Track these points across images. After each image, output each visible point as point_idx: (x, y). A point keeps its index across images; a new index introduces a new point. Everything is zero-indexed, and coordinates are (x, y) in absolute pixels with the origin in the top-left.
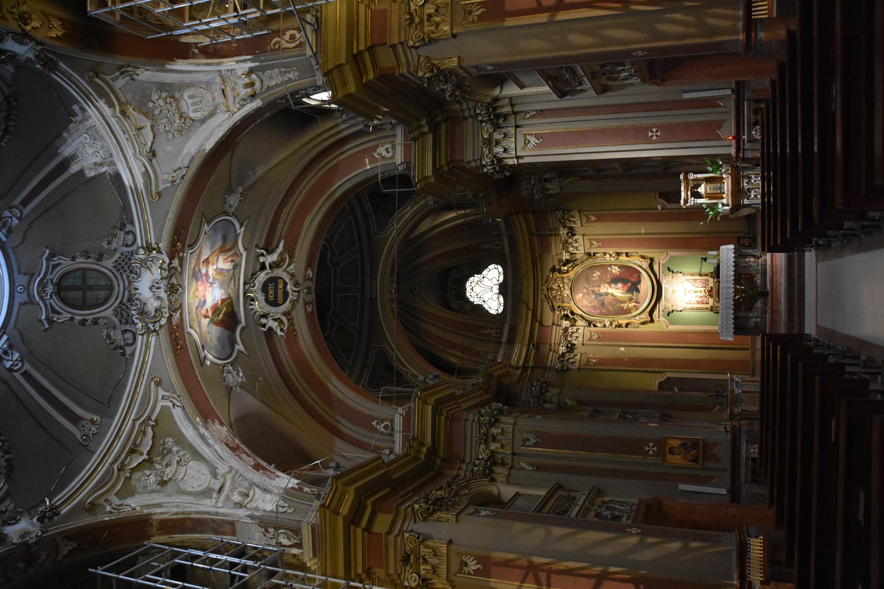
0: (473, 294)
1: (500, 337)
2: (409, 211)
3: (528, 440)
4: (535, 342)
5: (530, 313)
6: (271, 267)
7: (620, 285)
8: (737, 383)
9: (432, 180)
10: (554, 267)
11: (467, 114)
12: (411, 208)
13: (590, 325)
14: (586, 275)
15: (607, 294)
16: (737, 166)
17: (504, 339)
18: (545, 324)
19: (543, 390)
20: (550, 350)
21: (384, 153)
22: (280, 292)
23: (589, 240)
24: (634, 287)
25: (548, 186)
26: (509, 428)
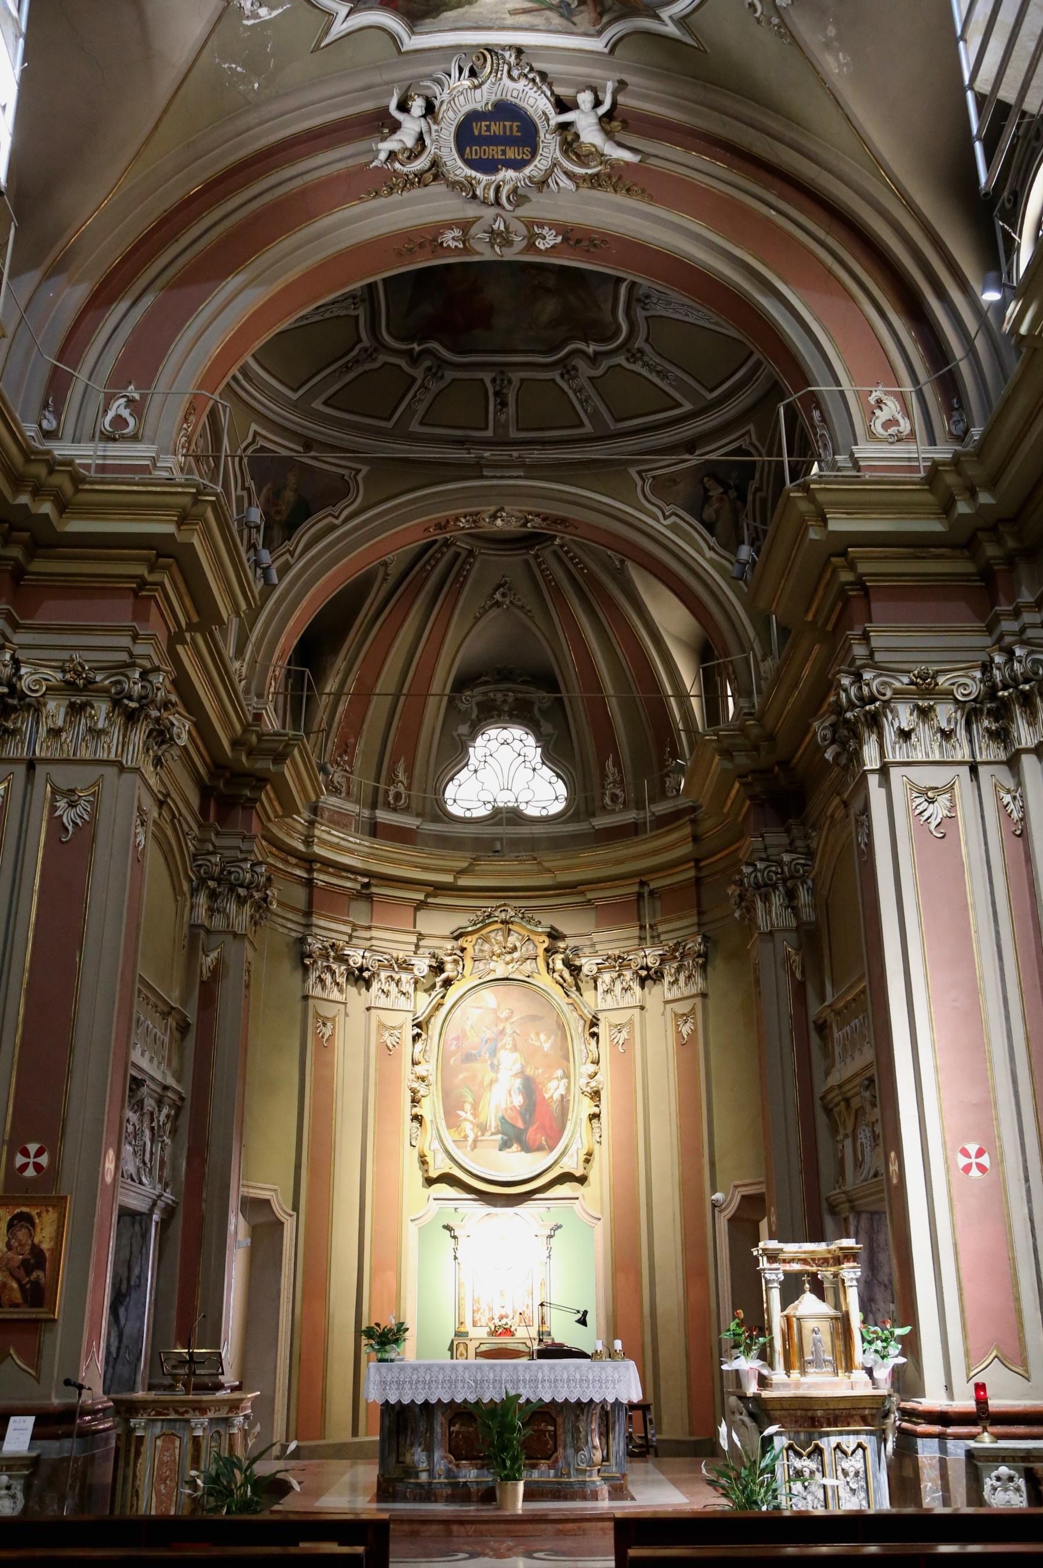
0: (493, 745)
1: (387, 806)
2: (701, 553)
3: (72, 805)
4: (374, 890)
5: (448, 878)
6: (564, 127)
7: (518, 1100)
8: (227, 1422)
9: (813, 535)
10: (562, 937)
11: (1008, 625)
12: (710, 561)
13: (418, 1025)
15: (495, 1068)
16: (886, 1415)
17: (383, 816)
19: (242, 892)
20: (355, 927)
21: (883, 416)
22: (494, 152)
23: (630, 1022)
24: (514, 1137)
25: (777, 900)
26: (109, 748)
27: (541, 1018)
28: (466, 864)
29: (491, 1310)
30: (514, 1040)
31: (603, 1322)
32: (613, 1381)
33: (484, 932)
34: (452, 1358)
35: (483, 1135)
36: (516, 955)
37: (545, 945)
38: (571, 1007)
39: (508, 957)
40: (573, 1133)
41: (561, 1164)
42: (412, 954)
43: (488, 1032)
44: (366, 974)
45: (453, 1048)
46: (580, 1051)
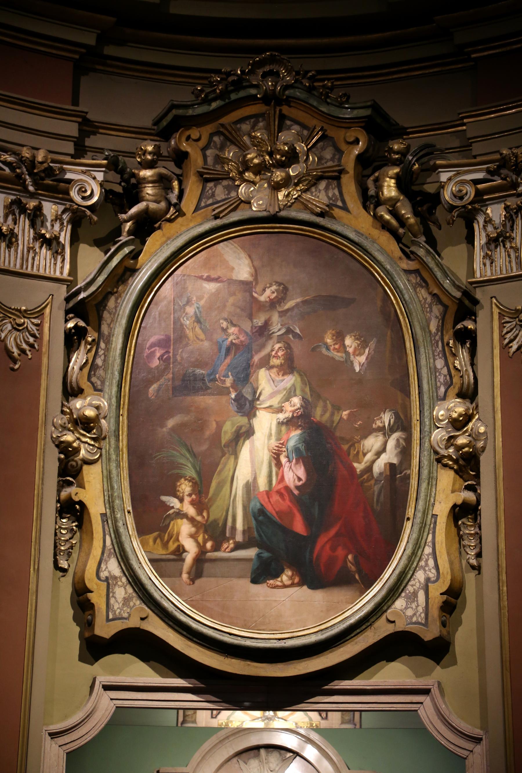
7: (294, 474)
14: (345, 285)
15: (247, 406)
18: (86, 83)
24: (282, 548)
27: (348, 302)
30: (288, 347)
33: (226, 120)
35: (217, 548)
38: (413, 279)
39: (278, 175)
40: (418, 546)
41: (389, 614)
43: (232, 330)
45: (155, 363)
46: (434, 371)
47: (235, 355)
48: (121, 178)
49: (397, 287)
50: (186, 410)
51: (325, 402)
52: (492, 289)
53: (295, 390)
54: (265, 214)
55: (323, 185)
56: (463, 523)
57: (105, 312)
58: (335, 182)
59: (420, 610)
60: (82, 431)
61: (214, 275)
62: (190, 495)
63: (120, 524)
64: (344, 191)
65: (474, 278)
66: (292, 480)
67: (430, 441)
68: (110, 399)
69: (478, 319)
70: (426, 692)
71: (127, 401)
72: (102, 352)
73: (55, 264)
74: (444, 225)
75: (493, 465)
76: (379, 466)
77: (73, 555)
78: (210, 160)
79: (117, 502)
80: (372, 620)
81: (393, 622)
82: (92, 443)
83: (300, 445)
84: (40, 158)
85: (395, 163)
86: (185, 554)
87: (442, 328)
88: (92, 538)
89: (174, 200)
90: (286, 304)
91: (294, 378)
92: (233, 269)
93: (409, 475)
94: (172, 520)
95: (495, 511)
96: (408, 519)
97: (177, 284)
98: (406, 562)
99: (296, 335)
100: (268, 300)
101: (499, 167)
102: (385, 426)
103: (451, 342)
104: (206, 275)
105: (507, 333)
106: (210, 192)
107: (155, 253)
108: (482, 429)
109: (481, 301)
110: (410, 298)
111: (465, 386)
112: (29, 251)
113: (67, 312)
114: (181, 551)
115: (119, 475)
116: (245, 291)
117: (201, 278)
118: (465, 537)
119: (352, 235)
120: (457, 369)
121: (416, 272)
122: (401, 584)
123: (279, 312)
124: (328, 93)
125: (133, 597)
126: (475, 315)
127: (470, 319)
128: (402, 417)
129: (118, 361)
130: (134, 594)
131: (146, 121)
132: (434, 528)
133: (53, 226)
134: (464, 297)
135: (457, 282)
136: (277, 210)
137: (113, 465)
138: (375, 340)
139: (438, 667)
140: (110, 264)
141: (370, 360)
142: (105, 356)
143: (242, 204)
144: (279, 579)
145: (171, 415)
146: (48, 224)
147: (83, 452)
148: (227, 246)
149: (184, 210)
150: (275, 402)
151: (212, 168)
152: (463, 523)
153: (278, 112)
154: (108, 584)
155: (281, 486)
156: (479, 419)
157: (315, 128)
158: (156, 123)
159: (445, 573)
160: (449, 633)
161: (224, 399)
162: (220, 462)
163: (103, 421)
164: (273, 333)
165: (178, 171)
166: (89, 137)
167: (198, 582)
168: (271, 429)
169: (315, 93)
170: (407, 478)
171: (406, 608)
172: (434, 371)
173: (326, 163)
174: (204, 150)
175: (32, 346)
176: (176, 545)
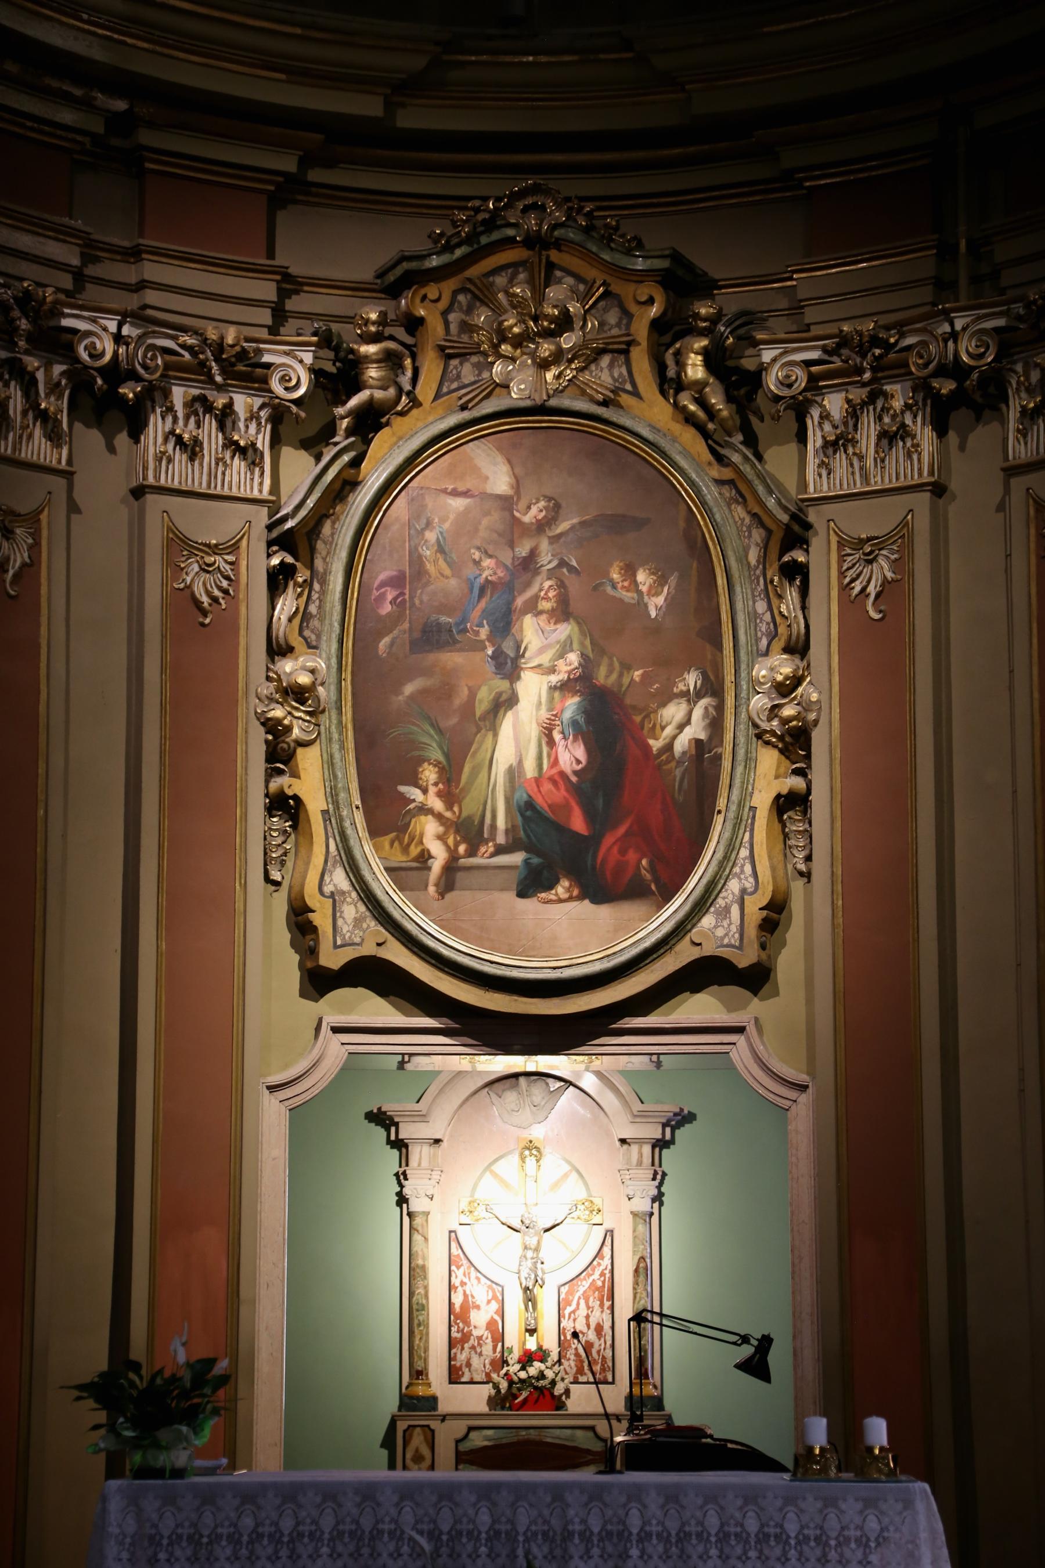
4: (147, 138)
5: (370, 106)
7: (571, 755)
10: (706, 287)
13: (284, 541)
14: (641, 508)
15: (509, 666)
20: (91, 251)
23: (902, 534)
24: (557, 852)
27: (640, 524)
28: (418, 62)
29: (499, 1337)
30: (561, 585)
31: (811, 1369)
32: (863, 1542)
33: (474, 271)
34: (392, 1466)
35: (472, 852)
36: (568, 341)
37: (654, 311)
38: (728, 492)
39: (546, 349)
40: (731, 848)
41: (694, 934)
42: (264, 334)
43: (487, 562)
44: (128, 391)
45: (386, 609)
46: (754, 617)
47: (491, 597)
48: (336, 356)
49: (704, 503)
50: (427, 672)
51: (611, 658)
52: (829, 509)
53: (571, 643)
54: (528, 403)
55: (605, 360)
56: (790, 818)
57: (319, 542)
58: (622, 357)
59: (734, 929)
60: (294, 703)
61: (461, 488)
62: (436, 784)
63: (347, 823)
64: (635, 370)
65: (806, 493)
66: (568, 763)
67: (748, 710)
68: (329, 659)
69: (810, 549)
70: (740, 1030)
71: (350, 660)
72: (317, 596)
73: (252, 479)
74: (767, 418)
75: (828, 743)
76: (682, 743)
77: (288, 863)
78: (454, 328)
79: (342, 795)
80: (673, 942)
81: (700, 944)
82: (308, 718)
83: (578, 717)
84: (230, 340)
85: (702, 333)
86: (431, 860)
87: (764, 559)
88: (311, 843)
89: (407, 387)
90: (557, 526)
91: (570, 628)
92: (487, 478)
93: (721, 754)
94: (414, 817)
95: (828, 805)
96: (719, 812)
97: (413, 500)
98: (716, 868)
99: (571, 569)
100: (534, 521)
101: (839, 346)
102: (689, 690)
103: (776, 579)
104: (450, 487)
105: (849, 569)
106: (454, 372)
107: (382, 460)
108: (814, 697)
109: (815, 525)
110: (722, 518)
111: (794, 638)
112: (217, 464)
113: (270, 544)
114: (426, 856)
115: (343, 759)
116: (503, 509)
117: (444, 491)
118: (791, 835)
119: (645, 432)
120: (783, 616)
121: (731, 482)
122: (709, 897)
123: (549, 537)
124: (611, 235)
125: (366, 917)
126: (807, 543)
127: (801, 548)
128: (712, 677)
129: (338, 607)
130: (368, 914)
131: (366, 273)
132: (753, 824)
133: (247, 427)
134: (793, 523)
135: (783, 501)
136: (545, 398)
137: (336, 747)
138: (676, 574)
139: (756, 1000)
140: (324, 478)
141: (670, 602)
142: (320, 601)
143: (498, 390)
144: (553, 892)
145: (410, 679)
146: (241, 425)
147: (296, 732)
148: (479, 447)
149: (420, 398)
150: (545, 659)
151: (455, 338)
152: (790, 818)
153: (544, 261)
154: (334, 901)
155: (554, 771)
156: (810, 683)
157: (594, 282)
158: (381, 275)
159: (766, 881)
160: (769, 957)
161: (477, 656)
162: (474, 740)
163: (320, 689)
164: (542, 566)
165: (409, 340)
166: (290, 298)
167: (449, 896)
168: (540, 697)
169: (594, 234)
170: (719, 757)
171: (716, 927)
172: (754, 617)
173: (610, 330)
174: (445, 314)
175: (226, 592)
176: (419, 849)
